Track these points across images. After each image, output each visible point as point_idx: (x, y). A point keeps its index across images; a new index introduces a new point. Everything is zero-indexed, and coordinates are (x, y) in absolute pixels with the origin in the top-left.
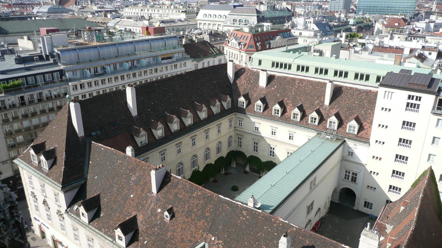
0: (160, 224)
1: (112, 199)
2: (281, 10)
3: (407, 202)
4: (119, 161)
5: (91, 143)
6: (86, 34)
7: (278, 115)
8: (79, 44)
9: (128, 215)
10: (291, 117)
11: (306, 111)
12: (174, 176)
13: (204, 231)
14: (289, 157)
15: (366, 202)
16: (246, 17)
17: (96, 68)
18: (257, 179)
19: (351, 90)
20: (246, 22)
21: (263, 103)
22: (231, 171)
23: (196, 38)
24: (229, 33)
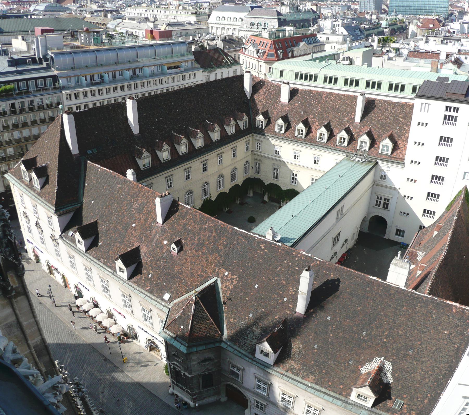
0: (166, 257)
1: (111, 227)
2: (305, 12)
3: (441, 226)
4: (118, 185)
5: (86, 163)
6: (83, 36)
7: (301, 136)
8: (75, 47)
9: (129, 246)
10: (316, 138)
11: (334, 131)
12: (182, 205)
13: (216, 265)
14: (314, 184)
15: (397, 230)
16: (265, 20)
17: (93, 76)
18: (277, 209)
19: (384, 103)
20: (265, 26)
21: (285, 122)
22: (248, 200)
23: (208, 44)
24: (245, 39)
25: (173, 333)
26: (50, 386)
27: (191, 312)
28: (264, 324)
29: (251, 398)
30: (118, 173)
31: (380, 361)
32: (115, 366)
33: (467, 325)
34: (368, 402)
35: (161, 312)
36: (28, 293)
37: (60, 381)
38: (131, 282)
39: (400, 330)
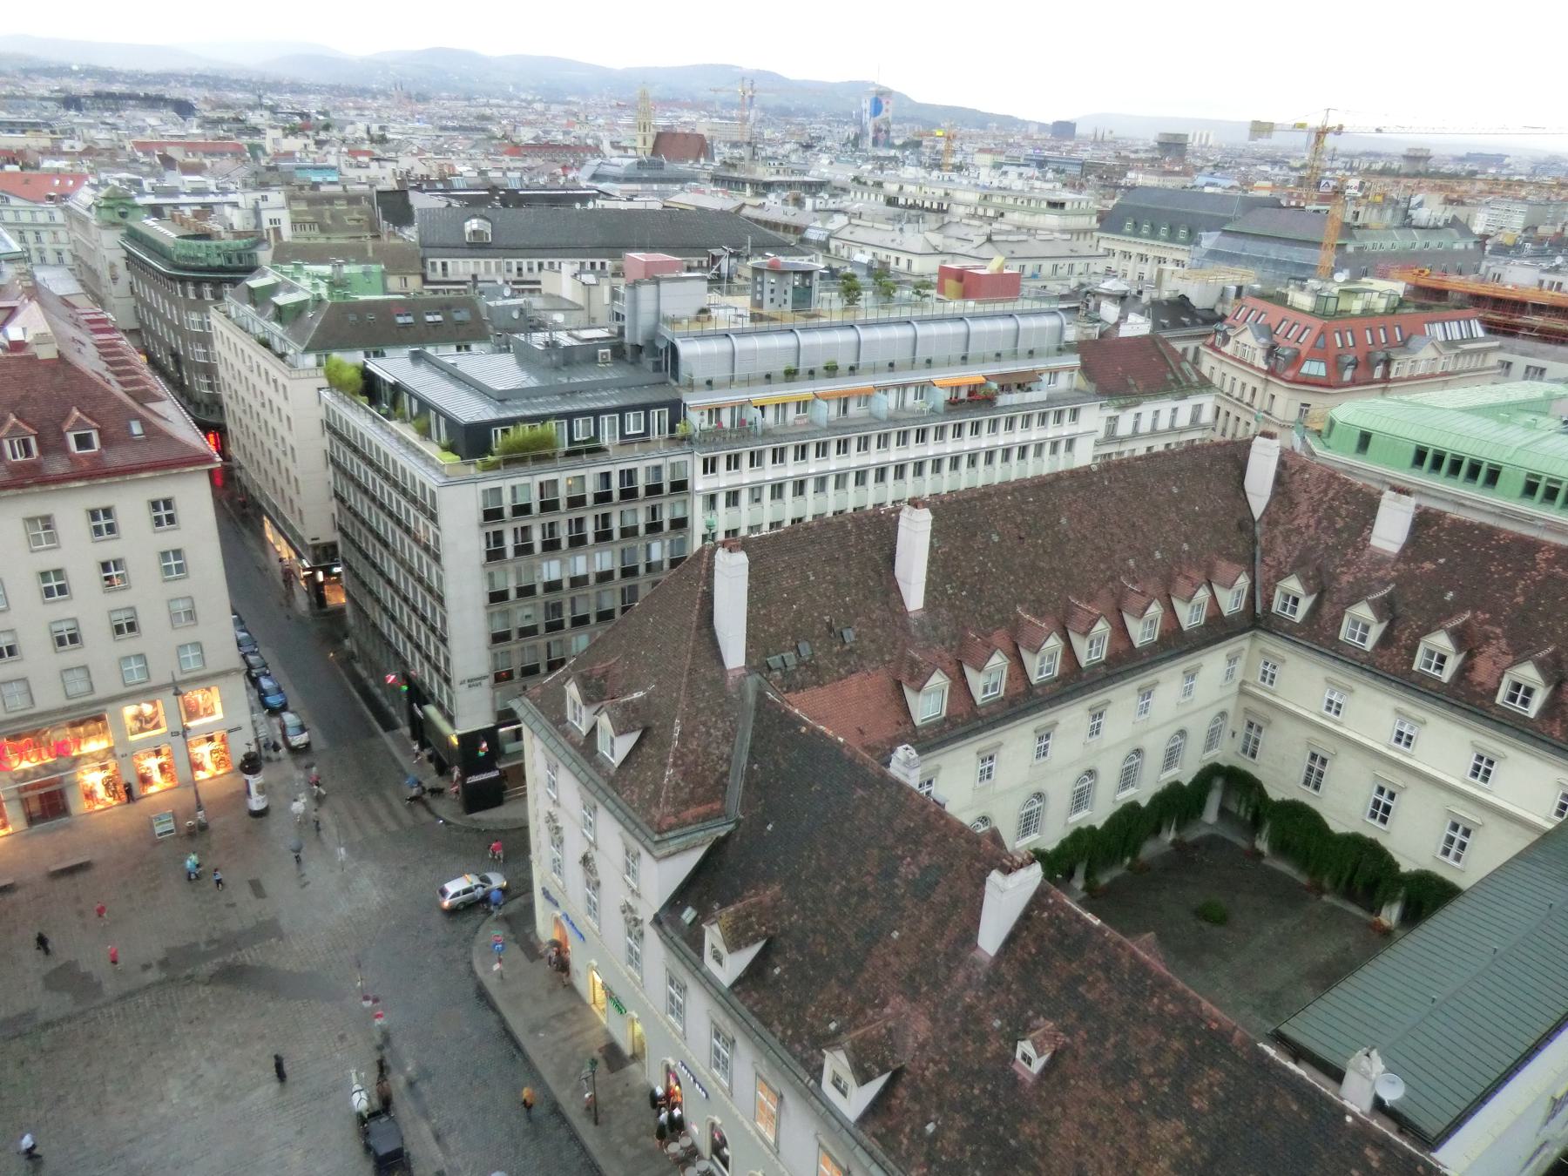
7: (1437, 673)
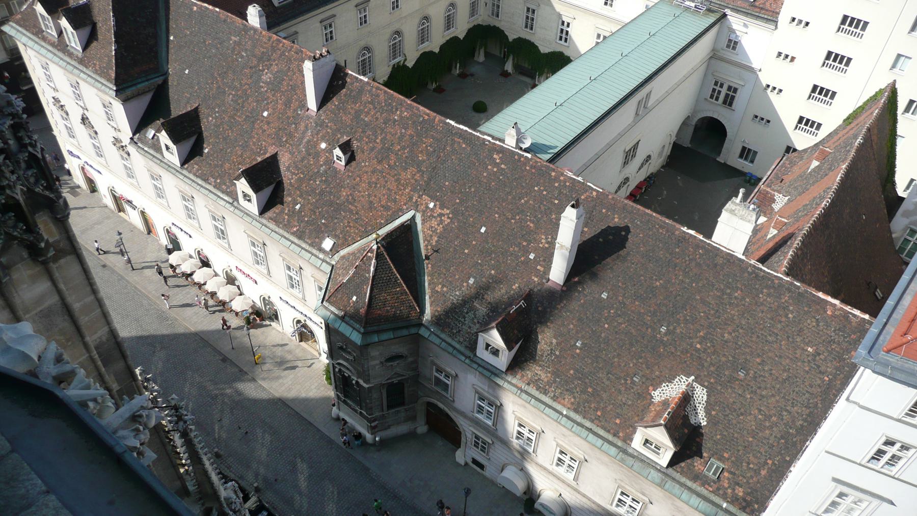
0: (326, 172)
1: (224, 118)
3: (827, 152)
4: (233, 38)
9: (259, 153)
12: (352, 75)
13: (414, 189)
14: (600, 46)
15: (744, 148)
22: (475, 69)
25: (339, 309)
26: (127, 415)
27: (369, 273)
28: (494, 298)
29: (467, 430)
30: (232, 13)
31: (687, 383)
32: (241, 370)
33: (851, 344)
34: (661, 455)
35: (319, 271)
36: (80, 249)
37: (145, 405)
38: (265, 219)
39: (727, 331)
